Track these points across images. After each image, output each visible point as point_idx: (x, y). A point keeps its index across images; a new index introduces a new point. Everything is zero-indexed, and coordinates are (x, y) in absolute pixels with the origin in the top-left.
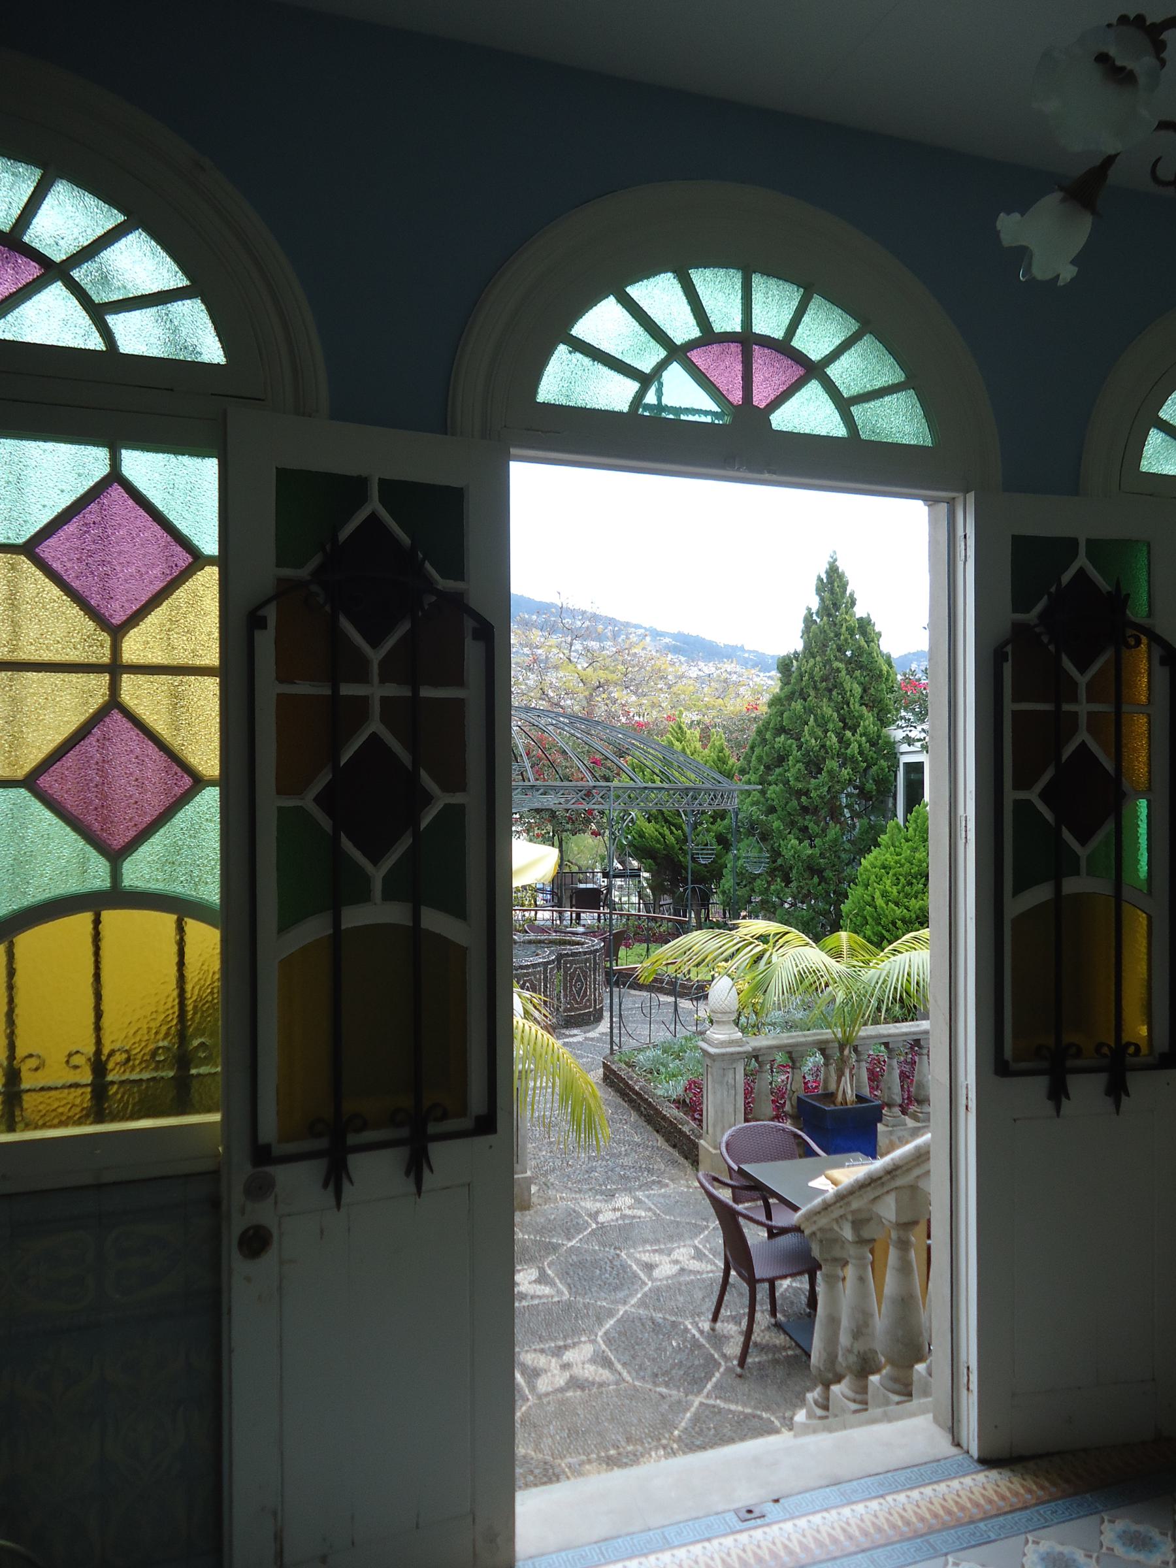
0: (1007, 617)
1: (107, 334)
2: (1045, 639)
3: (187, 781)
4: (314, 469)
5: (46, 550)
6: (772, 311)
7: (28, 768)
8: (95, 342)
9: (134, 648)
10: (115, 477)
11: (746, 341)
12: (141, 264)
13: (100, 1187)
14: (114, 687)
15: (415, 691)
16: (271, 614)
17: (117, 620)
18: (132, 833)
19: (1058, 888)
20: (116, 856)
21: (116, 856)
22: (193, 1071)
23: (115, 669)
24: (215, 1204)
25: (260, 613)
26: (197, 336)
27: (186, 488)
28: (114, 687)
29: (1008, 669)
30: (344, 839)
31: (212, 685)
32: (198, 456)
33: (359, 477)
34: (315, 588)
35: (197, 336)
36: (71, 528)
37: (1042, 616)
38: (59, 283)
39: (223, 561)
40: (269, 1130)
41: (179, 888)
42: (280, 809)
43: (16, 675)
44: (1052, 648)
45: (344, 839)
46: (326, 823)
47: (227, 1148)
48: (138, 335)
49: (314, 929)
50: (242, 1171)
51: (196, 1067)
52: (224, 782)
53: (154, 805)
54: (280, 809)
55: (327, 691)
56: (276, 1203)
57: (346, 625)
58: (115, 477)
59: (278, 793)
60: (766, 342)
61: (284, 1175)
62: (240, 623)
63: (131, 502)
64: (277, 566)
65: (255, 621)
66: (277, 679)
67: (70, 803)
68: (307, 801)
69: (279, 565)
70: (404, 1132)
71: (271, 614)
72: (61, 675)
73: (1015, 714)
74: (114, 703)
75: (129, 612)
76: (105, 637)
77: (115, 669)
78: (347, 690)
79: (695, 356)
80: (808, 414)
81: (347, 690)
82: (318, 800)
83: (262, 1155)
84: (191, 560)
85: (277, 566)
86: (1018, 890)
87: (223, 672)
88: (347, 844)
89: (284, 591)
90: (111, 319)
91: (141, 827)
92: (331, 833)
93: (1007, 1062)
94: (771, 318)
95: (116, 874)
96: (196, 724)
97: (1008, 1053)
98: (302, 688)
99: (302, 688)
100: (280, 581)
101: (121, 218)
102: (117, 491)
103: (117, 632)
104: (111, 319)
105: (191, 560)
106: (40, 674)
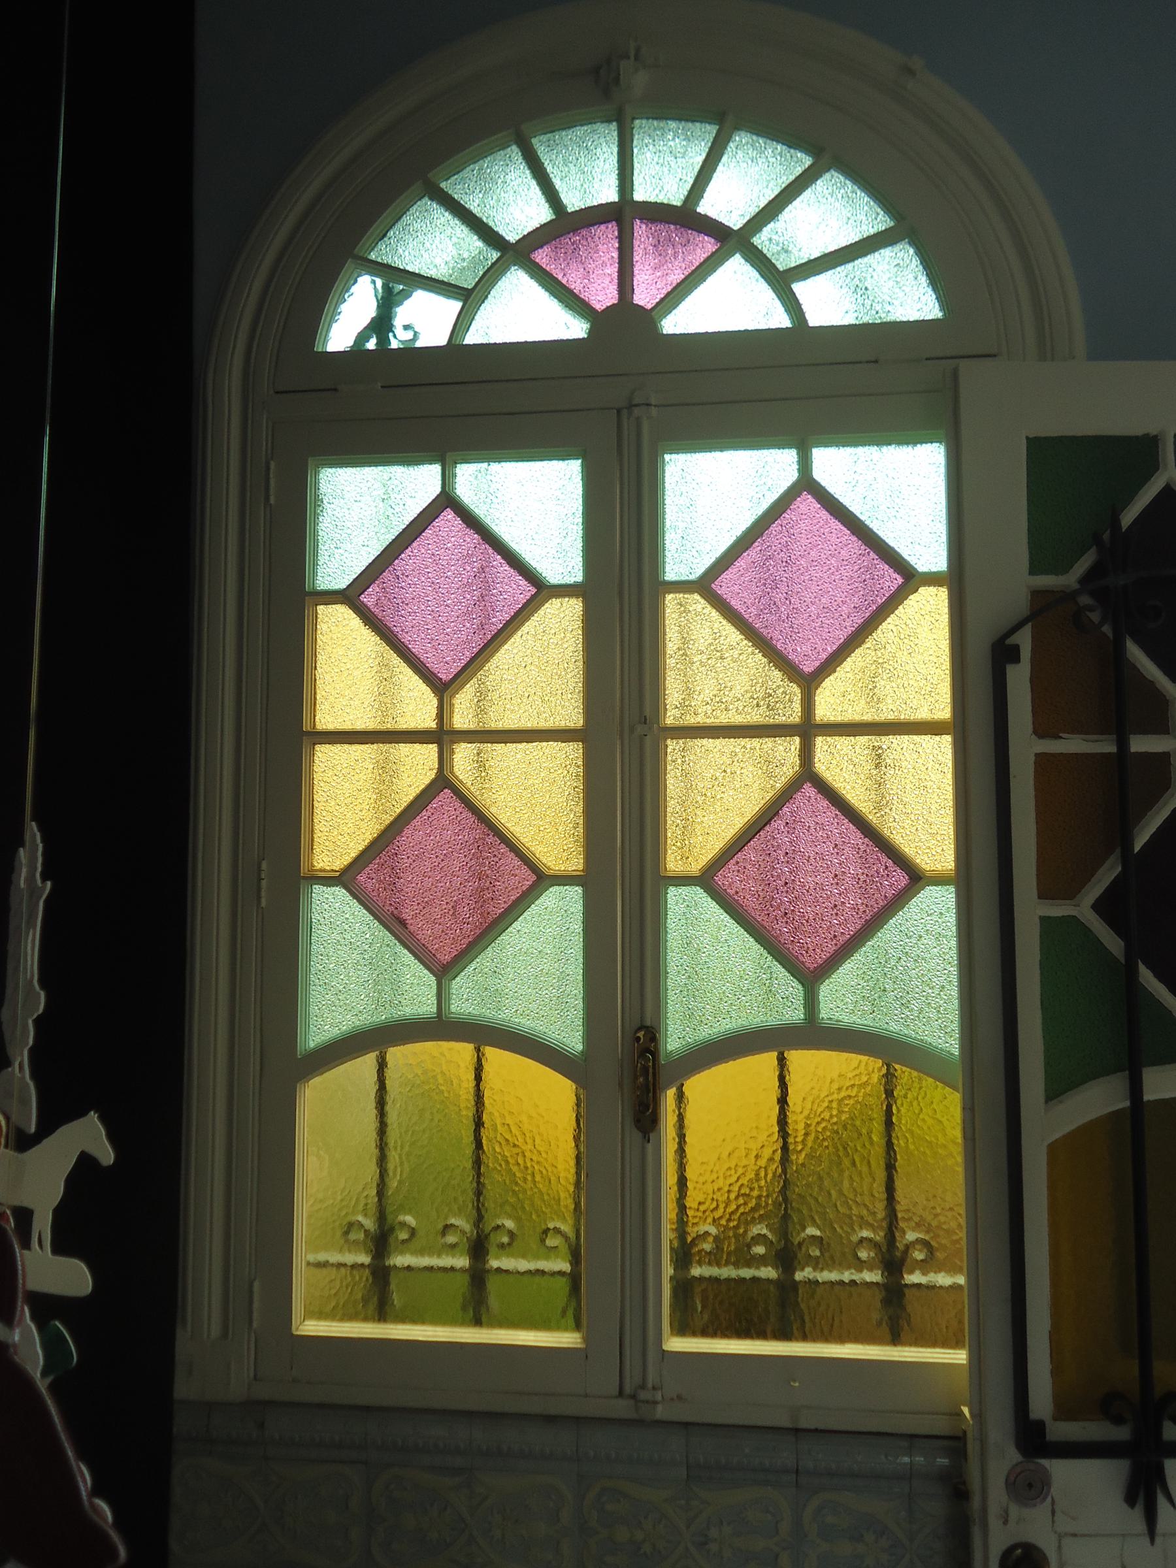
0: (1014, 582)
1: (793, 305)
2: (1095, 617)
3: (900, 879)
4: (1079, 433)
5: (725, 586)
6: (587, 174)
7: (347, 860)
8: (780, 319)
9: (834, 699)
10: (806, 484)
11: (566, 225)
12: (833, 212)
13: (797, 1432)
14: (807, 754)
15: (1123, 744)
16: (1024, 640)
17: (808, 667)
18: (831, 948)
19: (1136, 1088)
20: (811, 978)
21: (811, 978)
22: (494, 1263)
23: (807, 730)
24: (957, 1490)
25: (1010, 641)
26: (900, 291)
27: (902, 489)
28: (807, 754)
29: (1019, 677)
30: (1143, 969)
31: (942, 748)
32: (907, 443)
33: (1146, 436)
34: (1085, 600)
35: (900, 291)
36: (752, 554)
37: (1085, 580)
38: (738, 256)
39: (957, 579)
40: (1041, 1402)
41: (893, 1025)
42: (1043, 919)
43: (690, 743)
44: (1107, 629)
45: (1143, 969)
46: (1113, 944)
47: (978, 1415)
48: (828, 303)
49: (1100, 1099)
50: (1001, 1458)
51: (497, 1258)
52: (963, 878)
53: (854, 906)
54: (1043, 919)
55: (1108, 747)
56: (1053, 1513)
57: (1135, 652)
58: (806, 484)
59: (1039, 898)
60: (657, 213)
61: (1060, 1470)
62: (983, 662)
63: (824, 514)
64: (1031, 573)
65: (1003, 653)
66: (1035, 732)
67: (751, 904)
68: (1083, 907)
69: (1033, 571)
70: (1121, 1433)
71: (1024, 640)
72: (743, 741)
73: (1044, 762)
74: (808, 775)
75: (824, 656)
76: (795, 689)
77: (807, 730)
78: (1140, 744)
79: (542, 257)
80: (730, 303)
81: (1140, 744)
82: (1096, 907)
83: (1033, 1440)
84: (900, 580)
85: (1031, 573)
86: (1056, 1090)
87: (959, 727)
88: (1147, 977)
89: (1043, 606)
90: (799, 288)
91: (842, 940)
92: (1123, 960)
93: (1040, 1425)
94: (588, 179)
95: (811, 1002)
96: (919, 798)
97: (1041, 1402)
98: (1072, 745)
99: (1072, 745)
100: (1036, 594)
101: (807, 161)
102: (807, 503)
103: (809, 682)
104: (799, 288)
105: (900, 580)
106: (717, 741)
